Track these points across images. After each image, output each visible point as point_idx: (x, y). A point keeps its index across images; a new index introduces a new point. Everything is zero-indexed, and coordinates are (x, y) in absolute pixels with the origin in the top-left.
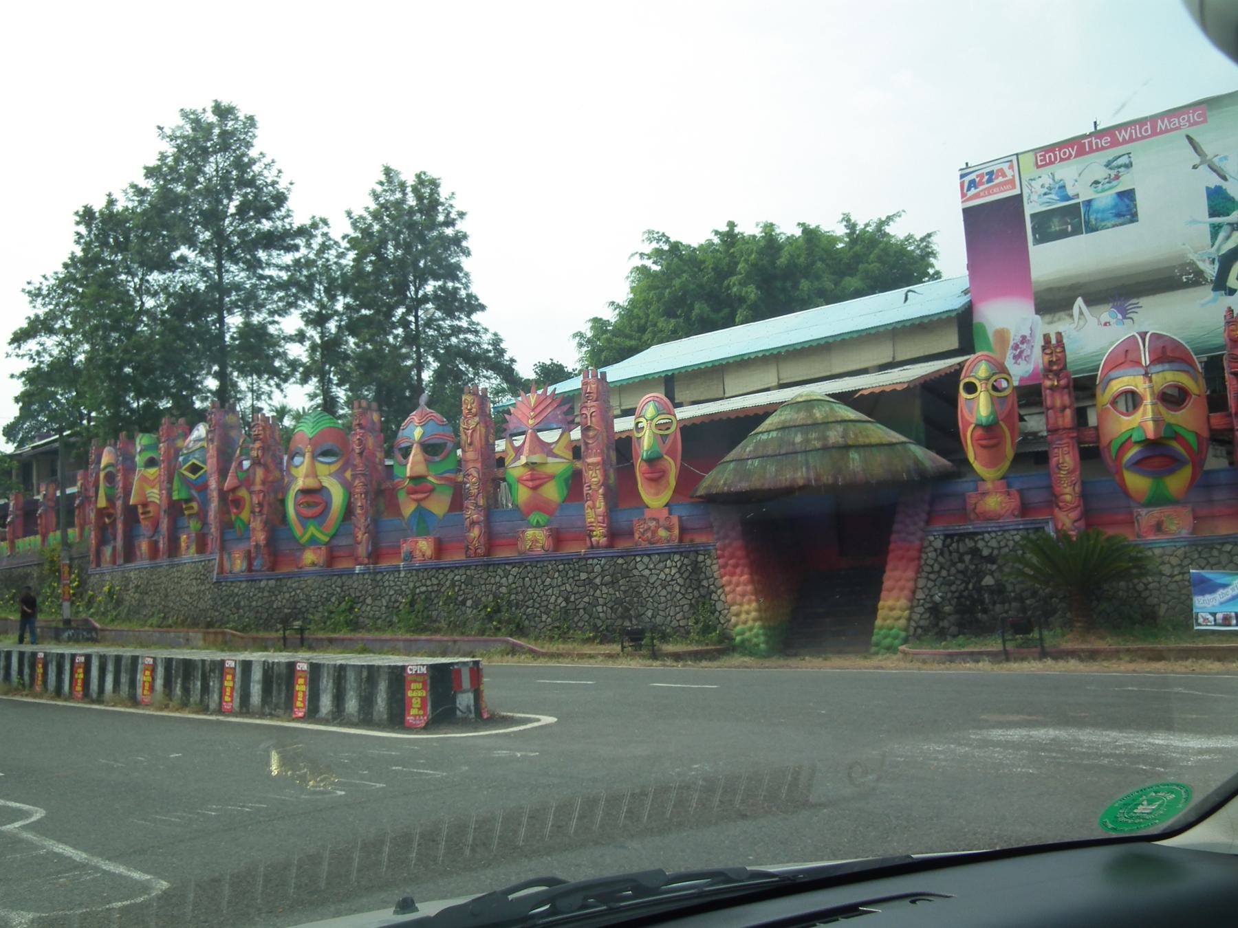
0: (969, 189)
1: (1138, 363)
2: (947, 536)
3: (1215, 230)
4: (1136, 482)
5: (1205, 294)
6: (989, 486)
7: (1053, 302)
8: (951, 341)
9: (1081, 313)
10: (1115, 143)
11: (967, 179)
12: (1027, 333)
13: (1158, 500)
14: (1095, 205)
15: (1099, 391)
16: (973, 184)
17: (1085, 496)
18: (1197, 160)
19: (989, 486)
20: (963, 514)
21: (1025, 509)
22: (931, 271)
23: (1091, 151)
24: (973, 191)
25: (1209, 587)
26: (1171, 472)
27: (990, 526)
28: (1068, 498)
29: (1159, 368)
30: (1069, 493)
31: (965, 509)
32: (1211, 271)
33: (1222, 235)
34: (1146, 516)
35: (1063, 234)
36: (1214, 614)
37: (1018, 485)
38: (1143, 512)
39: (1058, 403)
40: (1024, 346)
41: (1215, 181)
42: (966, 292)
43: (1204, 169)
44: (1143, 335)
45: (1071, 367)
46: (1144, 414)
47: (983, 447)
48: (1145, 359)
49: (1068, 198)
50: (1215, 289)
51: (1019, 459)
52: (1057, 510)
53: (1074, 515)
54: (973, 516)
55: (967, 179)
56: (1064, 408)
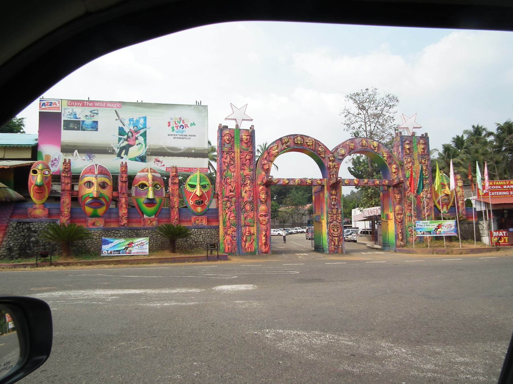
0: (42, 106)
1: (94, 173)
2: (18, 222)
3: (120, 139)
4: (89, 210)
5: (115, 157)
6: (37, 206)
7: (67, 149)
8: (29, 156)
9: (76, 155)
10: (94, 106)
11: (42, 102)
12: (57, 158)
13: (95, 216)
14: (85, 123)
15: (80, 180)
16: (44, 104)
17: (71, 212)
18: (117, 118)
19: (37, 206)
20: (26, 215)
21: (50, 215)
22: (22, 131)
23: (86, 106)
24: (44, 107)
25: (107, 243)
26: (100, 207)
27: (36, 220)
28: (66, 213)
29: (100, 176)
30: (66, 211)
31: (27, 213)
32: (117, 151)
33: (121, 141)
34: (91, 220)
35: (73, 129)
36: (108, 251)
37: (48, 207)
38: (90, 219)
39: (66, 182)
40: (56, 162)
41: (121, 125)
42: (36, 140)
43: (119, 121)
44: (96, 165)
45: (72, 171)
46: (94, 189)
47: (37, 193)
48: (96, 173)
49: (77, 118)
50: (118, 156)
51: (49, 198)
52: (61, 216)
53: (67, 218)
54: (29, 216)
55: (42, 102)
56: (68, 184)
